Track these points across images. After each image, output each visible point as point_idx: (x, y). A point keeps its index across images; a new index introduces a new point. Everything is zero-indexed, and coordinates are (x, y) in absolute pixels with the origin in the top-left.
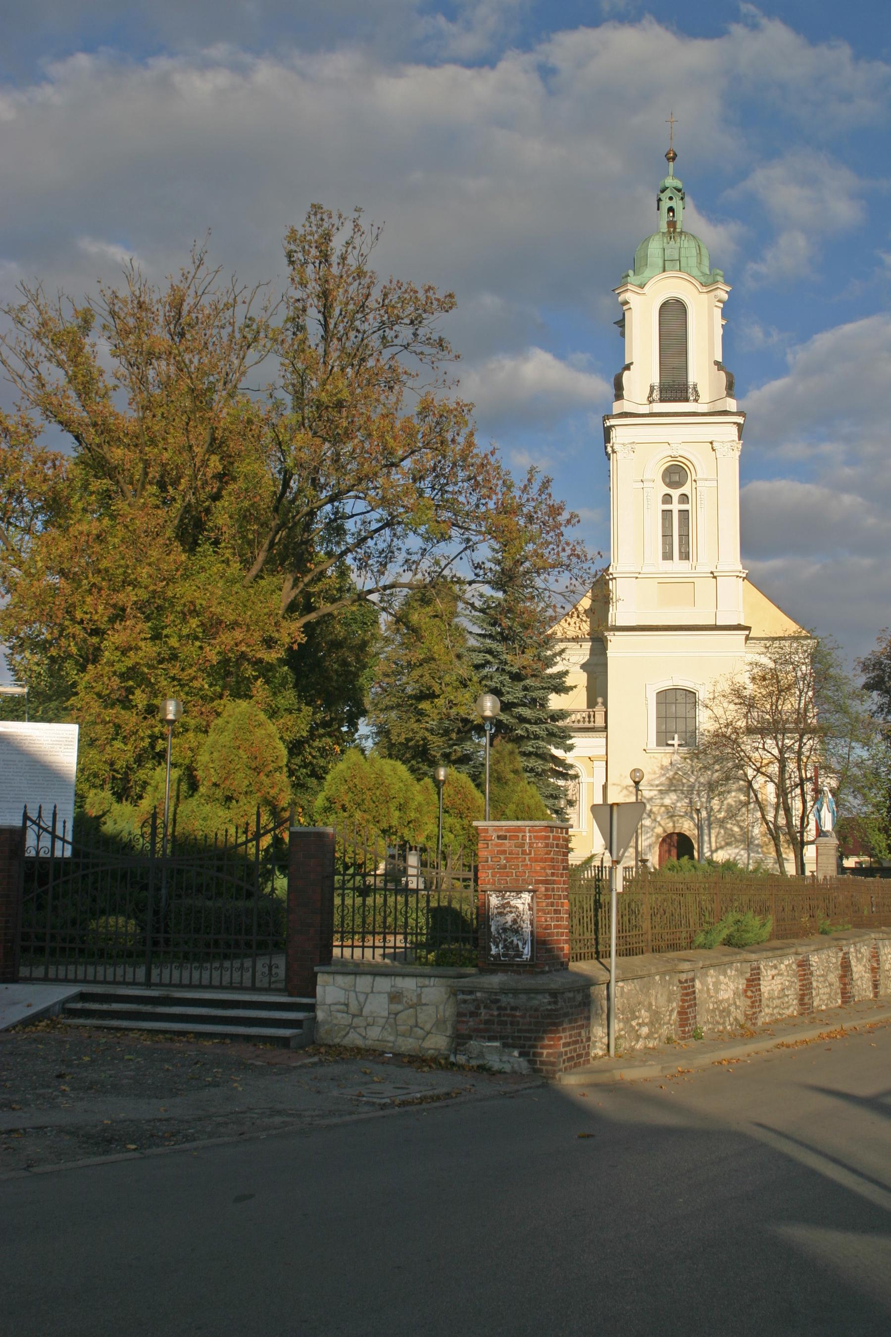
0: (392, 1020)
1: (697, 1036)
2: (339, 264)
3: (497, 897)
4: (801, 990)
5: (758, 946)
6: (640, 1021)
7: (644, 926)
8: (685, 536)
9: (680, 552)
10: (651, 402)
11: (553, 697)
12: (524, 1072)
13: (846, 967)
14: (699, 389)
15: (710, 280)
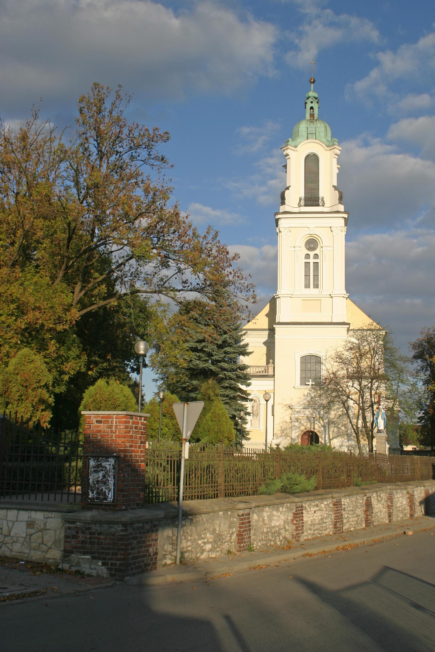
0: (28, 539)
1: (250, 549)
2: (108, 116)
3: (94, 460)
4: (335, 519)
5: (305, 492)
6: (206, 540)
7: (219, 481)
8: (316, 276)
9: (314, 284)
10: (299, 206)
11: (241, 357)
12: (105, 576)
13: (369, 505)
14: (325, 200)
15: (331, 144)
